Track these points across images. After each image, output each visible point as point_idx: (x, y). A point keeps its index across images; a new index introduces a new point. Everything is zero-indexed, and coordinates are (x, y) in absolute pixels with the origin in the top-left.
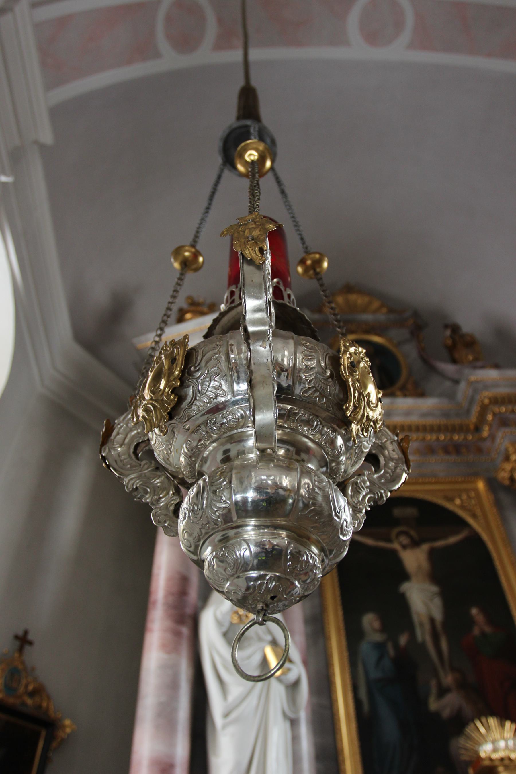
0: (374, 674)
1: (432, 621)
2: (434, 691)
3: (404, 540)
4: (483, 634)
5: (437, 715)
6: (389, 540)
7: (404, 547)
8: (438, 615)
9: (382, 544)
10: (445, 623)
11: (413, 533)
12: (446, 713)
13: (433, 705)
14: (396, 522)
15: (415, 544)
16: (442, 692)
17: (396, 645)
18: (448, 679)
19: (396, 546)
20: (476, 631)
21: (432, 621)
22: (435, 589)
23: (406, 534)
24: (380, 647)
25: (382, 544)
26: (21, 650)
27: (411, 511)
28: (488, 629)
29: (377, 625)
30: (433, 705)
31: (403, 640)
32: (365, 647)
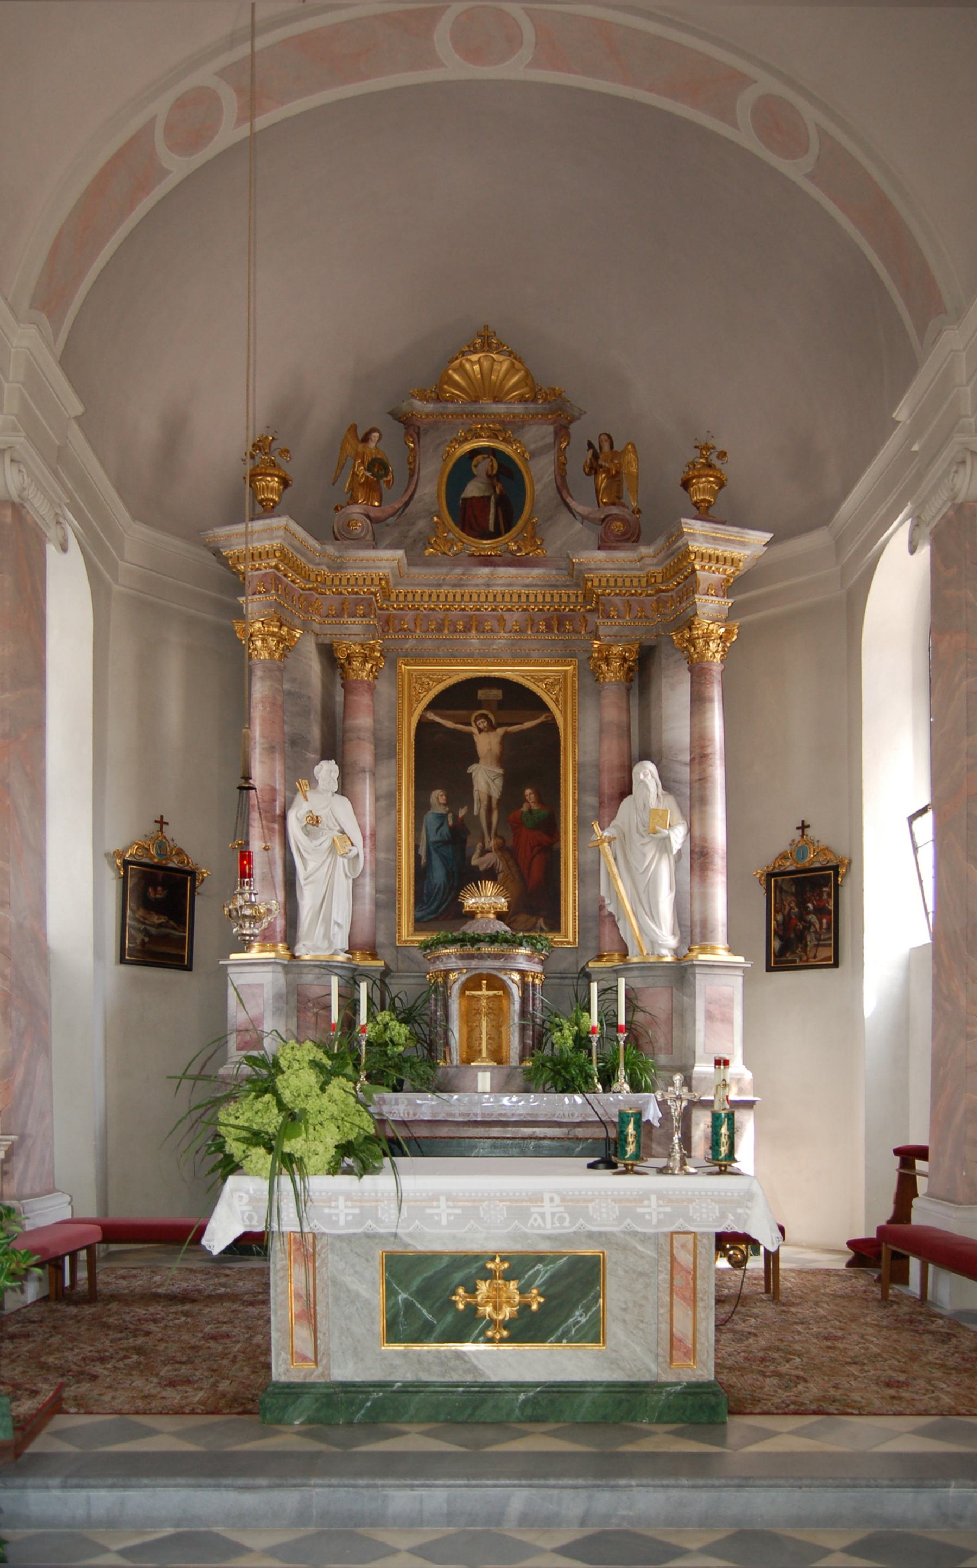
0: (434, 838)
1: (490, 798)
2: (478, 851)
3: (483, 723)
4: (530, 811)
5: (477, 867)
6: (469, 724)
7: (480, 731)
8: (496, 795)
9: (460, 727)
10: (499, 802)
11: (491, 717)
12: (482, 868)
13: (475, 861)
14: (479, 705)
15: (492, 727)
16: (484, 852)
17: (455, 817)
18: (491, 843)
19: (474, 729)
20: (525, 808)
21: (490, 798)
22: (500, 771)
23: (484, 716)
24: (442, 817)
25: (460, 727)
26: (161, 829)
27: (496, 694)
28: (535, 807)
29: (442, 800)
30: (475, 861)
31: (462, 813)
32: (429, 817)
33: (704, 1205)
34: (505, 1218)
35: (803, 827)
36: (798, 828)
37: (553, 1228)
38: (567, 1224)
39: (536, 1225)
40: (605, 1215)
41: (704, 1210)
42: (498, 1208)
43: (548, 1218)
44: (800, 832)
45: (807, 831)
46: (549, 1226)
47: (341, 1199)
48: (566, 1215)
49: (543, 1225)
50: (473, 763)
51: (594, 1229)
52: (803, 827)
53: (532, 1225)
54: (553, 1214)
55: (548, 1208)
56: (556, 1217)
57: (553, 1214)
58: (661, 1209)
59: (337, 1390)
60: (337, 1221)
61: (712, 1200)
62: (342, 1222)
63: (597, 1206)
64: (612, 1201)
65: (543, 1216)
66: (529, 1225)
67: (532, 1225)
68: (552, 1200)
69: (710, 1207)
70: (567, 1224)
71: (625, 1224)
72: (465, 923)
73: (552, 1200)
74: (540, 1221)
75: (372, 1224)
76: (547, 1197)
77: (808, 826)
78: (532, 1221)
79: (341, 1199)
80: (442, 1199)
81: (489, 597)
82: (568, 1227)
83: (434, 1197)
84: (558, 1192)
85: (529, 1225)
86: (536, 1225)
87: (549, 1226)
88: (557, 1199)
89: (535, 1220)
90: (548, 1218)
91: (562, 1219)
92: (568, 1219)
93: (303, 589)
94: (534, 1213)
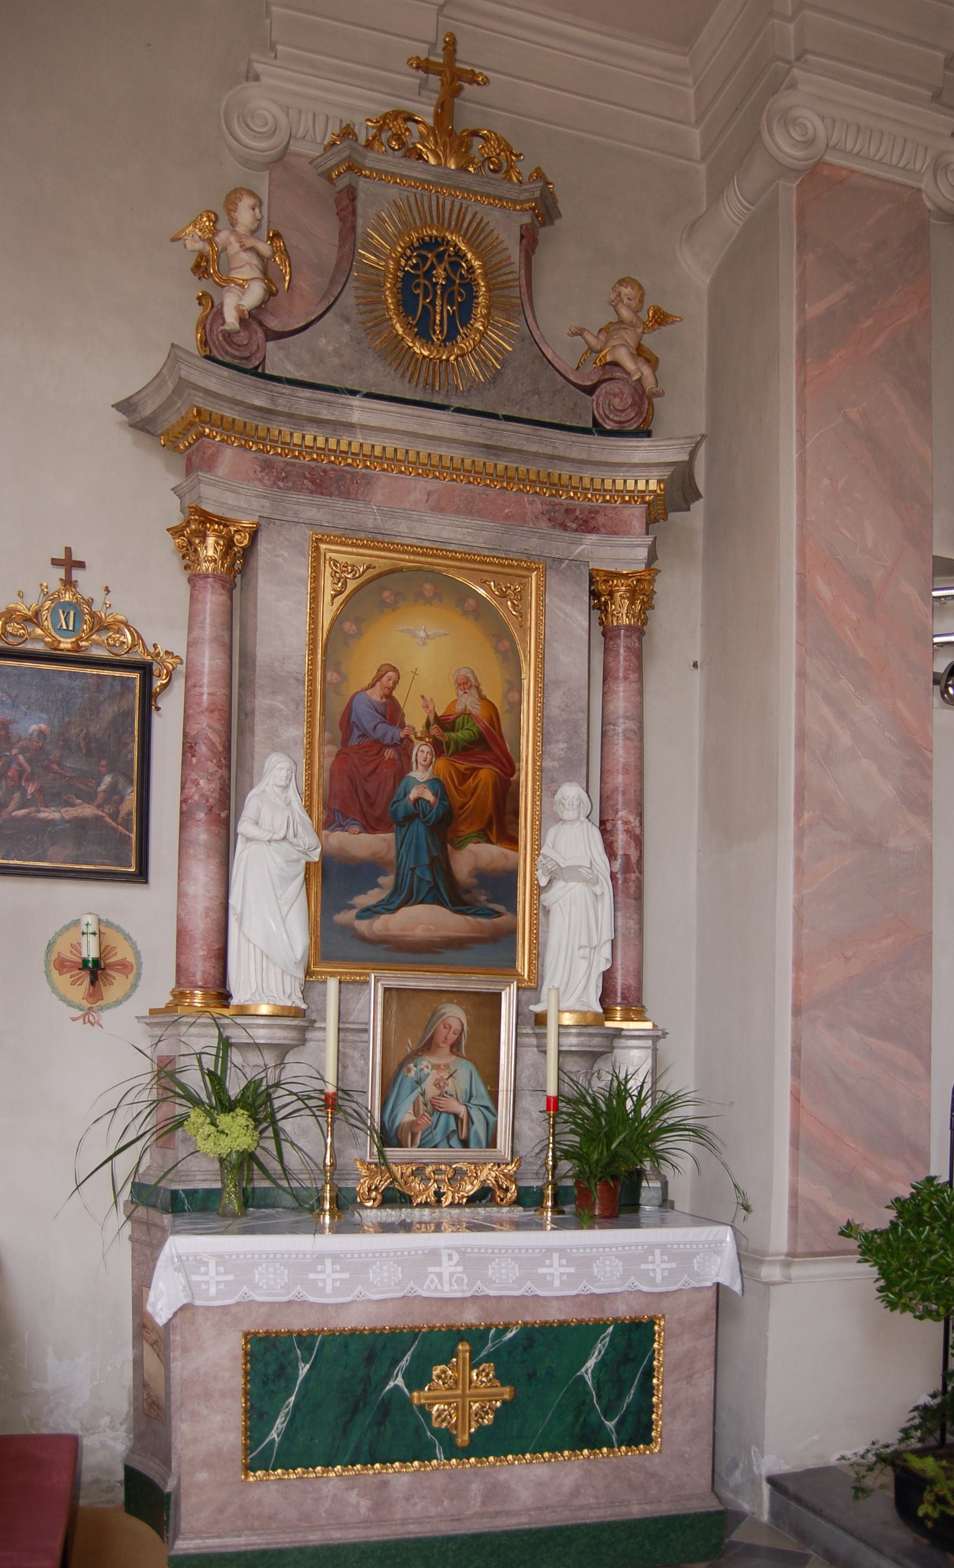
37: (452, 1291)
41: (504, 1271)
44: (61, 573)
50: (360, 894)
51: (492, 1293)
53: (428, 1287)
57: (452, 1274)
58: (651, 1266)
60: (324, 1288)
61: (616, 1257)
62: (659, 1279)
63: (279, 1280)
65: (439, 1275)
67: (428, 1287)
69: (264, 1281)
71: (581, 1287)
73: (450, 1256)
75: (481, 1285)
76: (445, 1254)
81: (398, 453)
84: (458, 1250)
85: (425, 1287)
86: (432, 1287)
88: (456, 1257)
92: (466, 1281)
93: (226, 114)
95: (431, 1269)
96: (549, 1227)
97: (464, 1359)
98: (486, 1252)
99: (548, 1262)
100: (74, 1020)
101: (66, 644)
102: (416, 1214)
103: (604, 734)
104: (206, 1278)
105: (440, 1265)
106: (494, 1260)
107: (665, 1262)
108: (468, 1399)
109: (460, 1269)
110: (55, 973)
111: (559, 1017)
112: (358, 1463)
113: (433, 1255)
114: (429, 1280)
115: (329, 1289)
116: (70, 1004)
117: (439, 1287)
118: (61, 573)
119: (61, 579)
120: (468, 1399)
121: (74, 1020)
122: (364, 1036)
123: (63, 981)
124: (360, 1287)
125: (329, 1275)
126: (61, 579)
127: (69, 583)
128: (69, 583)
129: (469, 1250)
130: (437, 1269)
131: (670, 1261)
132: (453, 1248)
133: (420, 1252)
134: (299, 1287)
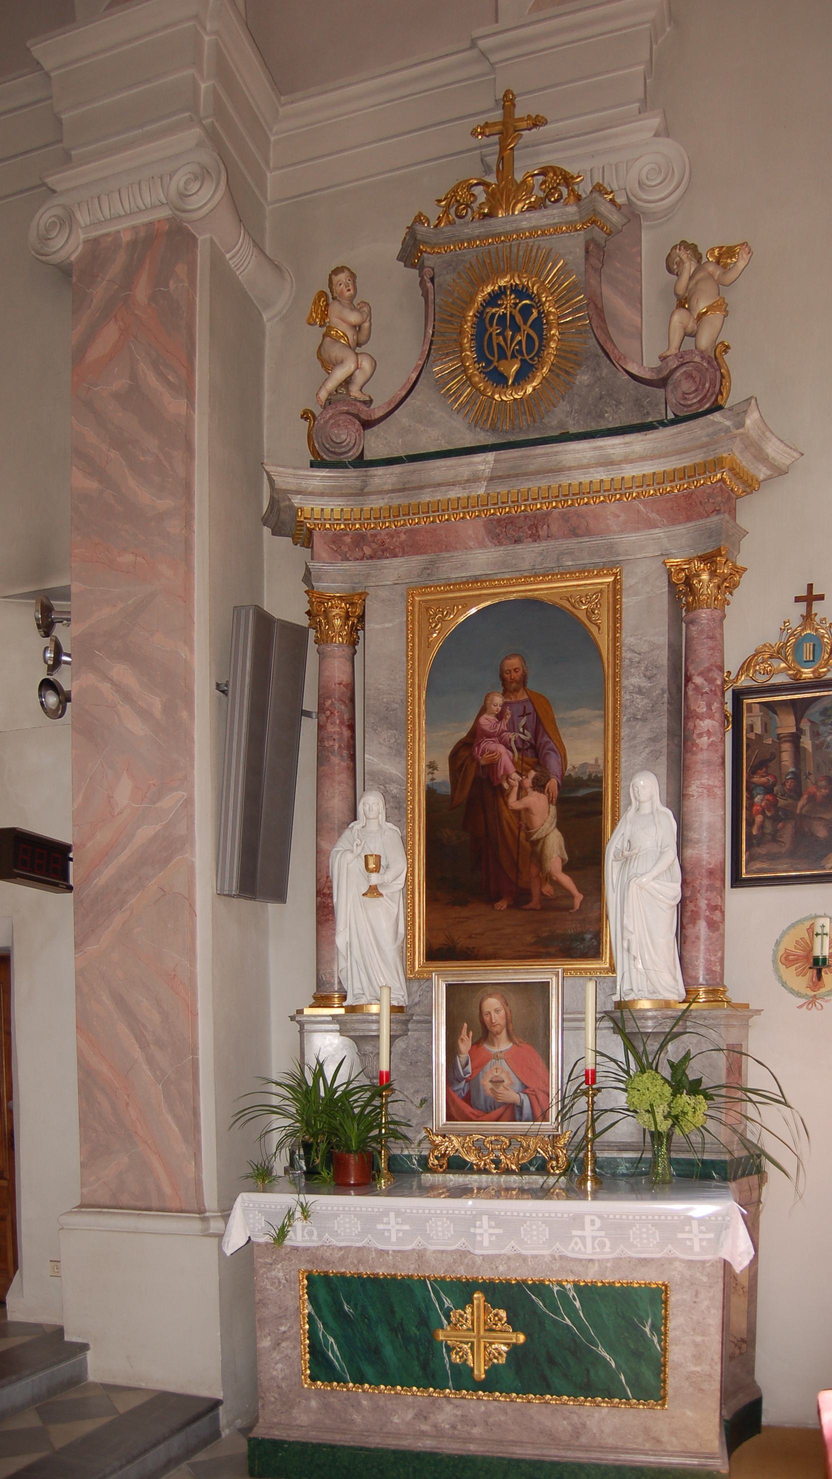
33: (644, 1230)
34: (359, 1232)
35: (810, 598)
36: (798, 599)
37: (304, 1241)
38: (607, 1249)
39: (577, 1249)
40: (440, 1234)
42: (650, 1232)
43: (589, 1242)
44: (802, 607)
45: (817, 606)
46: (589, 1250)
47: (485, 1218)
48: (606, 1240)
49: (583, 1250)
52: (810, 598)
53: (573, 1249)
54: (594, 1238)
55: (589, 1231)
56: (597, 1241)
59: (554, 1402)
60: (390, 1237)
61: (447, 1218)
64: (259, 1212)
65: (583, 1238)
66: (570, 1249)
67: (573, 1249)
68: (593, 1222)
70: (607, 1249)
72: (805, 749)
73: (593, 1222)
74: (580, 1245)
75: (371, 1238)
76: (587, 1219)
77: (821, 597)
78: (572, 1244)
79: (485, 1218)
80: (392, 1215)
82: (608, 1253)
83: (386, 1213)
85: (570, 1249)
86: (577, 1249)
87: (589, 1250)
89: (576, 1243)
90: (589, 1242)
91: (602, 1245)
92: (315, 1234)
94: (575, 1236)
95: (574, 1233)
96: (590, 1198)
97: (479, 1307)
98: (621, 1218)
99: (385, 1220)
100: (800, 1007)
101: (807, 673)
102: (473, 1180)
103: (724, 782)
104: (701, 1236)
105: (583, 1229)
106: (525, 1222)
107: (704, 1233)
108: (475, 1340)
109: (603, 1233)
110: (782, 967)
111: (381, 1009)
112: (589, 1397)
113: (577, 1220)
114: (573, 1242)
115: (697, 1248)
116: (798, 994)
117: (583, 1250)
118: (802, 607)
119: (802, 616)
120: (475, 1340)
121: (800, 1007)
122: (582, 1024)
123: (789, 974)
124: (558, 1244)
125: (486, 1231)
126: (802, 616)
127: (808, 617)
128: (808, 617)
129: (408, 1211)
130: (579, 1233)
131: (496, 1227)
132: (596, 1215)
133: (566, 1215)
134: (463, 1239)
